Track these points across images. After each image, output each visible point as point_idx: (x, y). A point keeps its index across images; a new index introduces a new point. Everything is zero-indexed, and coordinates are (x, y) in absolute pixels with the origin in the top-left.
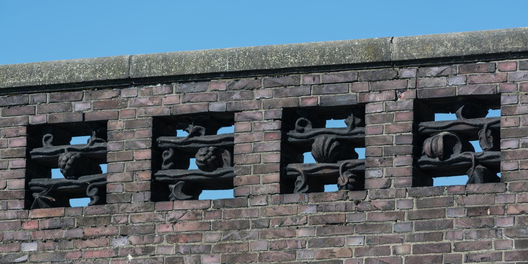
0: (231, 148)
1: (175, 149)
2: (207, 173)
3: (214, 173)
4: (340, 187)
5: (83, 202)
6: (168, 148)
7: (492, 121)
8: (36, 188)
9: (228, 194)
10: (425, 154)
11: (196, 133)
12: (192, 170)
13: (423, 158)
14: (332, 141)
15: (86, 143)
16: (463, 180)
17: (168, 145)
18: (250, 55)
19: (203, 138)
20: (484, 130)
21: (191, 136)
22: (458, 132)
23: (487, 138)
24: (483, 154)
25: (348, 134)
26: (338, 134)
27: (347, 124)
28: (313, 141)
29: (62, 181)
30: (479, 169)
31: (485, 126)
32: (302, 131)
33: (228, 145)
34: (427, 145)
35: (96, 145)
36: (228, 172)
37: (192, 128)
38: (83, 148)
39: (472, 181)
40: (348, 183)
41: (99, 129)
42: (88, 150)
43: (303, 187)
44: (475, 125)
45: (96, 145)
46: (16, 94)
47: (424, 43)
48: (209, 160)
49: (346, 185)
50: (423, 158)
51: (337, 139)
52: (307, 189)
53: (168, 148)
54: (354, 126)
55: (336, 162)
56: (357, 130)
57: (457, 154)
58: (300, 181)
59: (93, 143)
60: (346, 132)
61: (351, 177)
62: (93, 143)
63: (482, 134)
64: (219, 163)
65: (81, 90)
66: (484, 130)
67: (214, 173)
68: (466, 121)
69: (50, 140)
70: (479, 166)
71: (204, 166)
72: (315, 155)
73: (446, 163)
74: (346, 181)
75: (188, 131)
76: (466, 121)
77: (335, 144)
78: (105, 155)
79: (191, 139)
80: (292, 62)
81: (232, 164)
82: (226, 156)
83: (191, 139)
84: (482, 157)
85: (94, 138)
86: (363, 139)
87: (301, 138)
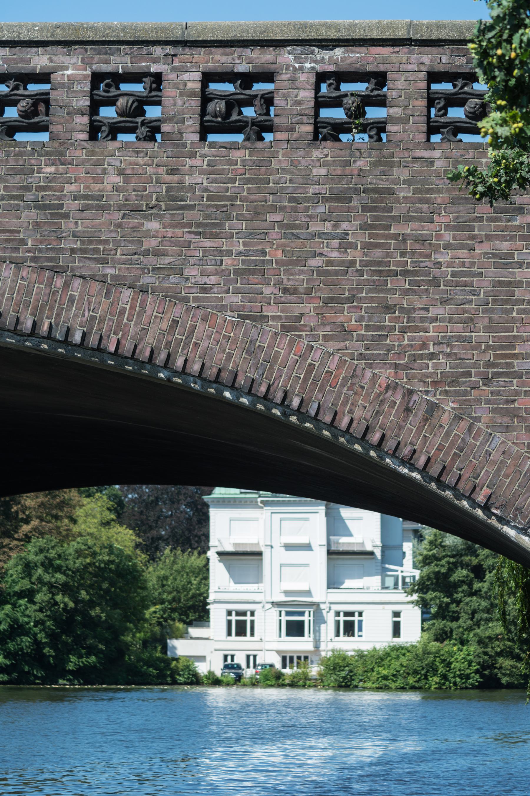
0: (47, 102)
1: (445, 99)
2: (25, 121)
3: (32, 121)
4: (138, 139)
5: (131, 138)
6: (439, 99)
7: (265, 92)
8: (322, 125)
9: (44, 137)
10: (208, 114)
11: (16, 88)
12: (6, 118)
13: (207, 118)
14: (133, 102)
15: (364, 90)
16: (239, 138)
17: (440, 96)
18: (158, 29)
19: (21, 92)
20: (259, 99)
21: (12, 90)
22: (237, 100)
23: (261, 105)
24: (257, 118)
25: (147, 97)
26: (138, 96)
27: (145, 89)
28: (118, 100)
29: (343, 121)
30: (255, 129)
31: (259, 96)
32: (108, 92)
33: (44, 99)
34: (211, 107)
35: (376, 92)
36: (44, 121)
37: (12, 83)
38: (448, 92)
39: (247, 139)
40: (146, 136)
41: (380, 79)
42: (368, 96)
43: (107, 136)
44: (252, 95)
45: (376, 92)
46: (42, 47)
47: (428, 26)
48: (29, 111)
49: (144, 138)
50: (207, 118)
51: (137, 100)
52: (110, 137)
53: (439, 99)
54: (151, 90)
55: (135, 117)
56: (154, 93)
57: (234, 117)
58: (105, 131)
59: (372, 91)
60: (145, 95)
61: (148, 131)
62: (372, 91)
63: (257, 102)
64: (36, 113)
65: (38, 47)
66: (259, 99)
67: (32, 121)
68: (244, 92)
69: (333, 86)
70: (254, 127)
71: (24, 115)
72: (118, 111)
73: (226, 123)
74: (144, 135)
75: (8, 86)
76: (244, 92)
77: (136, 104)
78: (385, 100)
79: (13, 93)
80: (153, 37)
81: (47, 114)
82: (42, 108)
83: (13, 93)
84: (257, 120)
85: (373, 87)
86: (161, 101)
87: (107, 97)
